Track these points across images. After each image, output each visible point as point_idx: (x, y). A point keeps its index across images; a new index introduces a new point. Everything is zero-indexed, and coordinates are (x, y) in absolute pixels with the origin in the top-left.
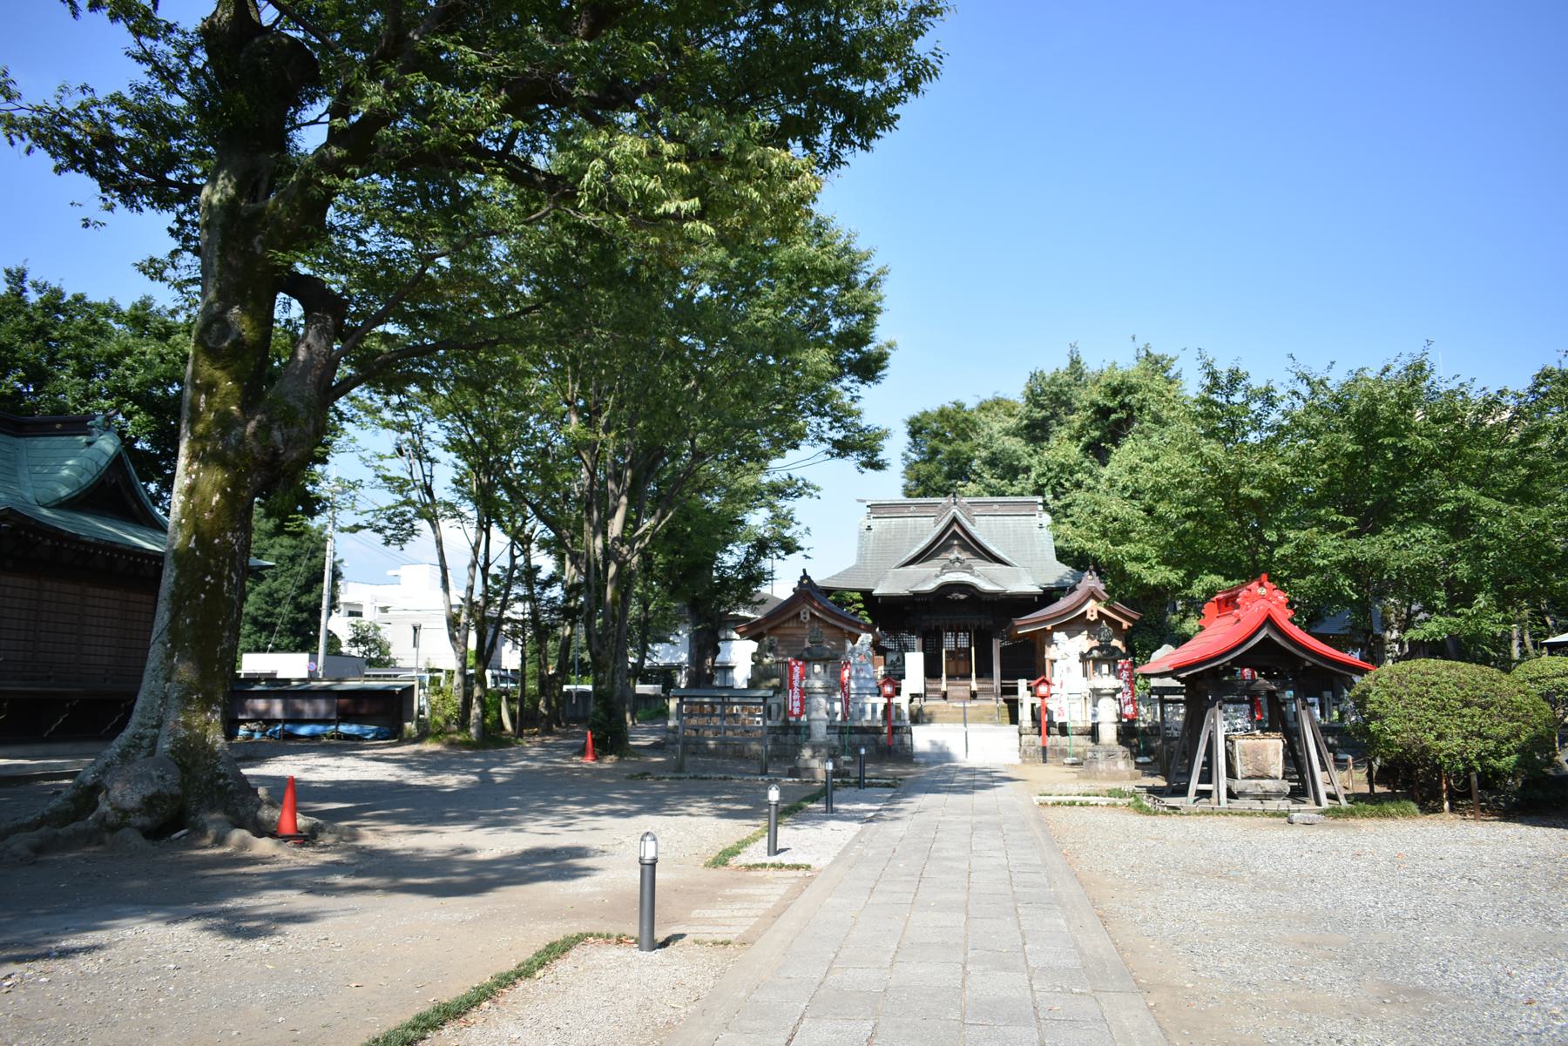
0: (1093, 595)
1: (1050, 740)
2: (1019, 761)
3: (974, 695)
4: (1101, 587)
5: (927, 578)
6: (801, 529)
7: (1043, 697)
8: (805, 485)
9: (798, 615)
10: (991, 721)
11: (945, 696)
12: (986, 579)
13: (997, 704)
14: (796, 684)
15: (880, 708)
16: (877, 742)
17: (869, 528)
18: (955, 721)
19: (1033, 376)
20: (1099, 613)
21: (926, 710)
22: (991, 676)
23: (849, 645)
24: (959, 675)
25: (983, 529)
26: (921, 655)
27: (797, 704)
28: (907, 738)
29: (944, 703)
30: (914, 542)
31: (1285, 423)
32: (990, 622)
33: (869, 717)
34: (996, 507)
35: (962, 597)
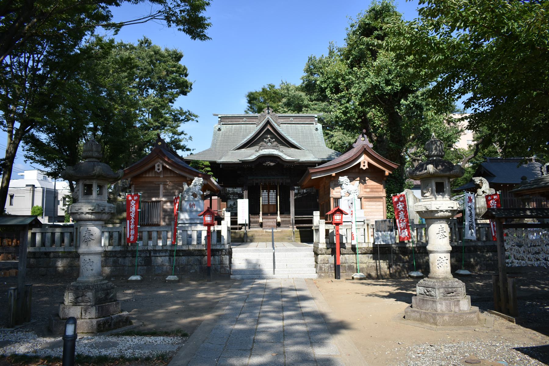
0: (365, 151)
1: (342, 258)
2: (315, 276)
3: (279, 225)
4: (371, 145)
5: (251, 154)
6: (187, 137)
7: (337, 224)
8: (190, 115)
9: (154, 167)
10: (289, 240)
11: (261, 225)
12: (287, 155)
13: (291, 230)
14: (399, 226)
15: (204, 234)
16: (200, 263)
17: (219, 130)
18: (267, 241)
19: (310, 59)
20: (369, 164)
21: (249, 234)
22: (288, 212)
23: (186, 187)
24: (270, 211)
25: (284, 130)
26: (247, 200)
27: (133, 232)
28: (226, 258)
29: (261, 229)
30: (244, 137)
32: (289, 181)
33: (195, 243)
34: (291, 119)
35: (272, 164)
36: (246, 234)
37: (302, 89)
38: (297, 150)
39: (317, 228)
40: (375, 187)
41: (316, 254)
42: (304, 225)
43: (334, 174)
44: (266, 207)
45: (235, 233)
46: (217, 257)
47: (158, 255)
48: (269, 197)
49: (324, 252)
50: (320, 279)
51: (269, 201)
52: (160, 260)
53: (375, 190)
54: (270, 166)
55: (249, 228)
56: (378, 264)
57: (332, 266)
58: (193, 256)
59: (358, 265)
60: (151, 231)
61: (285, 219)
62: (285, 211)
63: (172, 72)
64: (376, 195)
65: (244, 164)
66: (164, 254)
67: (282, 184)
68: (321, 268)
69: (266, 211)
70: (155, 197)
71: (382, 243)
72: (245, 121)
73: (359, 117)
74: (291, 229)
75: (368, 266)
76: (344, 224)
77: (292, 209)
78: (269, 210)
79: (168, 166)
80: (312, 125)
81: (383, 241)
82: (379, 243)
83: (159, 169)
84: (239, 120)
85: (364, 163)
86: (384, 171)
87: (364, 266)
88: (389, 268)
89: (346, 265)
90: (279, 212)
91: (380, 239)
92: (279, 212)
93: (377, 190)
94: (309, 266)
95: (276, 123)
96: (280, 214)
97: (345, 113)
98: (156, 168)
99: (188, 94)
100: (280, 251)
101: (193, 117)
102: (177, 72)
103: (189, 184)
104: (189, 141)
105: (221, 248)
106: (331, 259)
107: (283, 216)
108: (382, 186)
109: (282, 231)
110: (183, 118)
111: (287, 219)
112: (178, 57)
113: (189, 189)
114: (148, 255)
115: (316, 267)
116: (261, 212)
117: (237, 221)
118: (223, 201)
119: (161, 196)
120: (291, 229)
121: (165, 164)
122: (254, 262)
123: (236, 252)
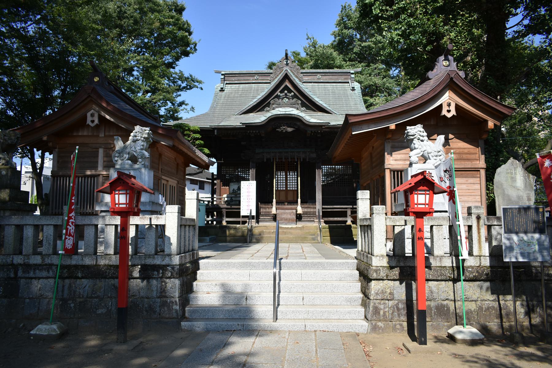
0: (450, 84)
2: (363, 326)
3: (299, 218)
6: (188, 108)
7: (420, 215)
13: (316, 226)
17: (222, 90)
19: (344, 8)
21: (256, 231)
22: (313, 200)
23: (119, 144)
24: (287, 199)
26: (255, 182)
30: (254, 97)
31: (529, 18)
32: (314, 155)
34: (319, 76)
35: (290, 130)
36: (250, 230)
37: (333, 47)
38: (326, 114)
39: (366, 223)
40: (466, 151)
41: (365, 277)
42: (336, 219)
43: (392, 126)
45: (235, 228)
46: (154, 282)
47: (31, 274)
48: (286, 180)
49: (383, 274)
50: (374, 336)
51: (286, 185)
52: (37, 286)
53: (464, 156)
54: (286, 132)
55: (258, 222)
56: (502, 302)
57: (401, 306)
58: (105, 278)
59: (458, 304)
60: (23, 225)
61: (308, 210)
63: (169, 24)
64: (468, 165)
65: (249, 127)
66: (44, 274)
67: (304, 159)
68: (376, 311)
69: (283, 198)
70: (91, 168)
71: (521, 259)
72: (257, 79)
73: (429, 42)
74: (316, 224)
75: (481, 308)
76: (435, 215)
77: (319, 196)
78: (286, 198)
79: (108, 117)
80: (346, 84)
81: (522, 255)
82: (514, 260)
83: (93, 121)
84: (248, 78)
85: (449, 105)
86: (486, 121)
87: (473, 306)
88: (529, 313)
89: (433, 304)
90: (299, 200)
91: (517, 251)
92: (299, 200)
93: (469, 156)
94: (350, 301)
95: (297, 77)
96: (301, 202)
97: (404, 35)
98: (89, 119)
99: (191, 55)
100: (291, 266)
101: (196, 84)
102: (175, 24)
103: (125, 140)
104: (191, 112)
105: (164, 263)
106: (400, 290)
107: (306, 206)
108: (478, 150)
109: (303, 227)
110: (184, 85)
111: (311, 210)
112: (180, 10)
113: (125, 147)
114: (12, 275)
115: (364, 304)
116: (274, 200)
117: (240, 212)
118: (224, 185)
119: (100, 168)
120: (316, 224)
121: (103, 114)
122: (239, 289)
123: (207, 268)
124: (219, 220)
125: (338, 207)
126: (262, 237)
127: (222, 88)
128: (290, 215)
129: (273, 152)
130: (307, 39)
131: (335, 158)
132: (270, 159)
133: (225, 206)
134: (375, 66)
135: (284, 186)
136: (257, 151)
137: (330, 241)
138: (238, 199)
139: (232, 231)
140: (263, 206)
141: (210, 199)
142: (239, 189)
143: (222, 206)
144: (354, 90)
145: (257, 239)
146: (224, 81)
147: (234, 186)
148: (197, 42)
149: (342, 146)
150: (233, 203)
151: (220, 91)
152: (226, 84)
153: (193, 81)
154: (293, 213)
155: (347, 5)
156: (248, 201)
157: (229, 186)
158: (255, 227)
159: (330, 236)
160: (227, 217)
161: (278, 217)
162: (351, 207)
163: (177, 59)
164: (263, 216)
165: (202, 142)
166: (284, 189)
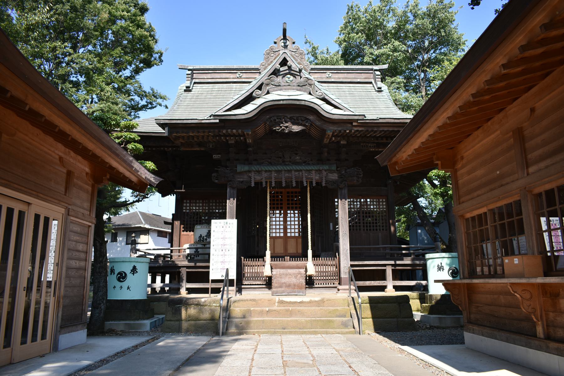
3: (310, 282)
11: (269, 283)
17: (188, 89)
19: (351, 8)
21: (237, 310)
26: (235, 221)
32: (334, 177)
34: (328, 74)
35: (296, 128)
44: (279, 243)
51: (285, 229)
54: (290, 132)
55: (239, 291)
62: (326, 247)
69: (280, 250)
78: (286, 249)
90: (310, 252)
92: (310, 252)
96: (314, 256)
101: (159, 101)
109: (322, 301)
110: (143, 103)
112: (144, 10)
116: (268, 253)
118: (186, 230)
124: (174, 286)
125: (371, 264)
126: (248, 323)
127: (187, 87)
128: (296, 277)
129: (266, 171)
130: (306, 43)
131: (396, 163)
132: (261, 183)
133: (186, 263)
134: (393, 79)
135: (282, 231)
136: (240, 168)
137: (372, 327)
138: (206, 251)
139: (192, 311)
140: (250, 263)
141: (168, 252)
142: (209, 234)
143: (180, 264)
144: (381, 91)
145: (237, 326)
146: (192, 79)
147: (200, 230)
148: (163, 51)
149: (431, 131)
150: (200, 258)
151: (185, 91)
152: (195, 83)
153: (155, 97)
154: (300, 273)
155: (354, 5)
156: (223, 257)
157: (193, 231)
158: (235, 302)
159: (373, 317)
160: (188, 281)
161: (274, 281)
162: (393, 262)
163: (137, 71)
164: (249, 279)
165: (140, 146)
166: (282, 235)
